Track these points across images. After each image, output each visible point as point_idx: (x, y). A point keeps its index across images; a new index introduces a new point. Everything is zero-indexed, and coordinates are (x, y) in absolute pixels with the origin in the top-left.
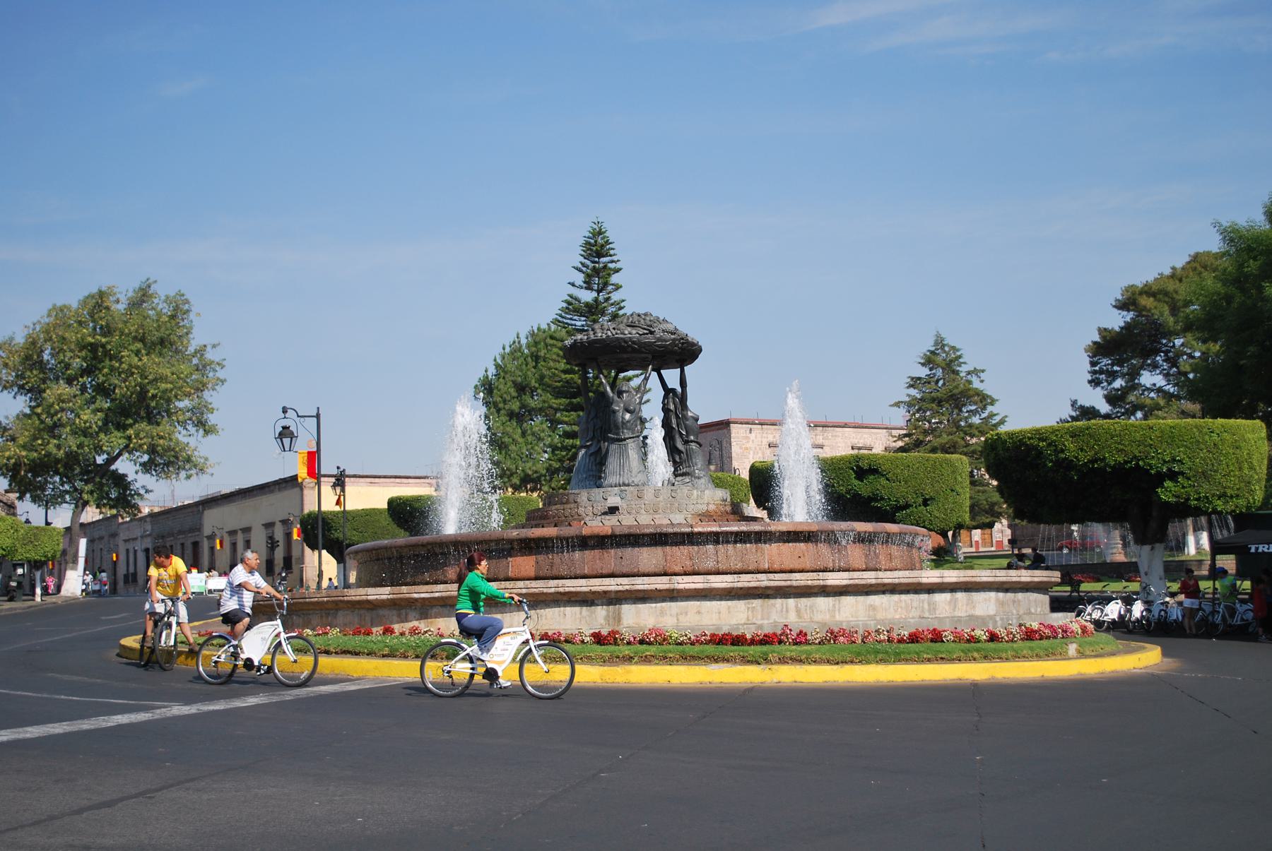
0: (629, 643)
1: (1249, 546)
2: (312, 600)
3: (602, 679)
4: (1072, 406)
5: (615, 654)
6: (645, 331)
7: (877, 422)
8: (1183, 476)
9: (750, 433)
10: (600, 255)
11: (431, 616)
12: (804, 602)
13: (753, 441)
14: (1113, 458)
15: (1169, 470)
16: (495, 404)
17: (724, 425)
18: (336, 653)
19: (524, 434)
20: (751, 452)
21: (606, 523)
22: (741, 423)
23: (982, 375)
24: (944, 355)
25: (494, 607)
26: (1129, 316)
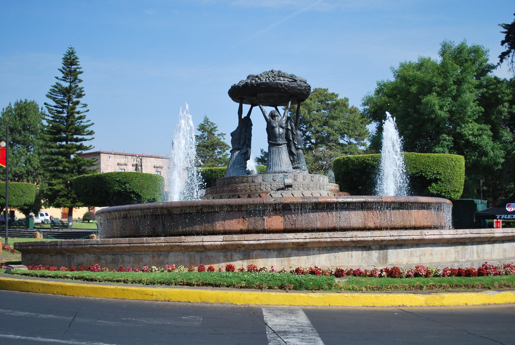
0: (408, 276)
1: (496, 215)
2: (151, 244)
3: (426, 304)
4: (261, 151)
5: (413, 284)
6: (293, 80)
8: (440, 181)
9: (110, 158)
10: (72, 64)
11: (252, 257)
12: (480, 247)
13: (110, 162)
15: (435, 178)
17: (98, 154)
18: (198, 285)
20: (110, 167)
21: (284, 195)
22: (106, 153)
23: (224, 136)
24: (208, 126)
25: (302, 250)
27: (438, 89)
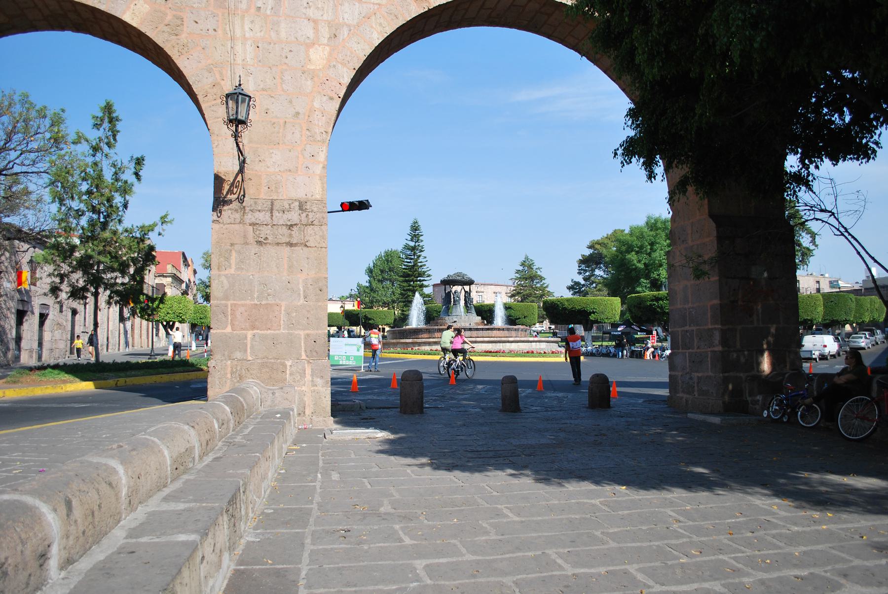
7: (503, 284)
10: (416, 230)
12: (504, 344)
14: (578, 307)
16: (373, 277)
19: (383, 287)
26: (591, 251)
27: (637, 249)
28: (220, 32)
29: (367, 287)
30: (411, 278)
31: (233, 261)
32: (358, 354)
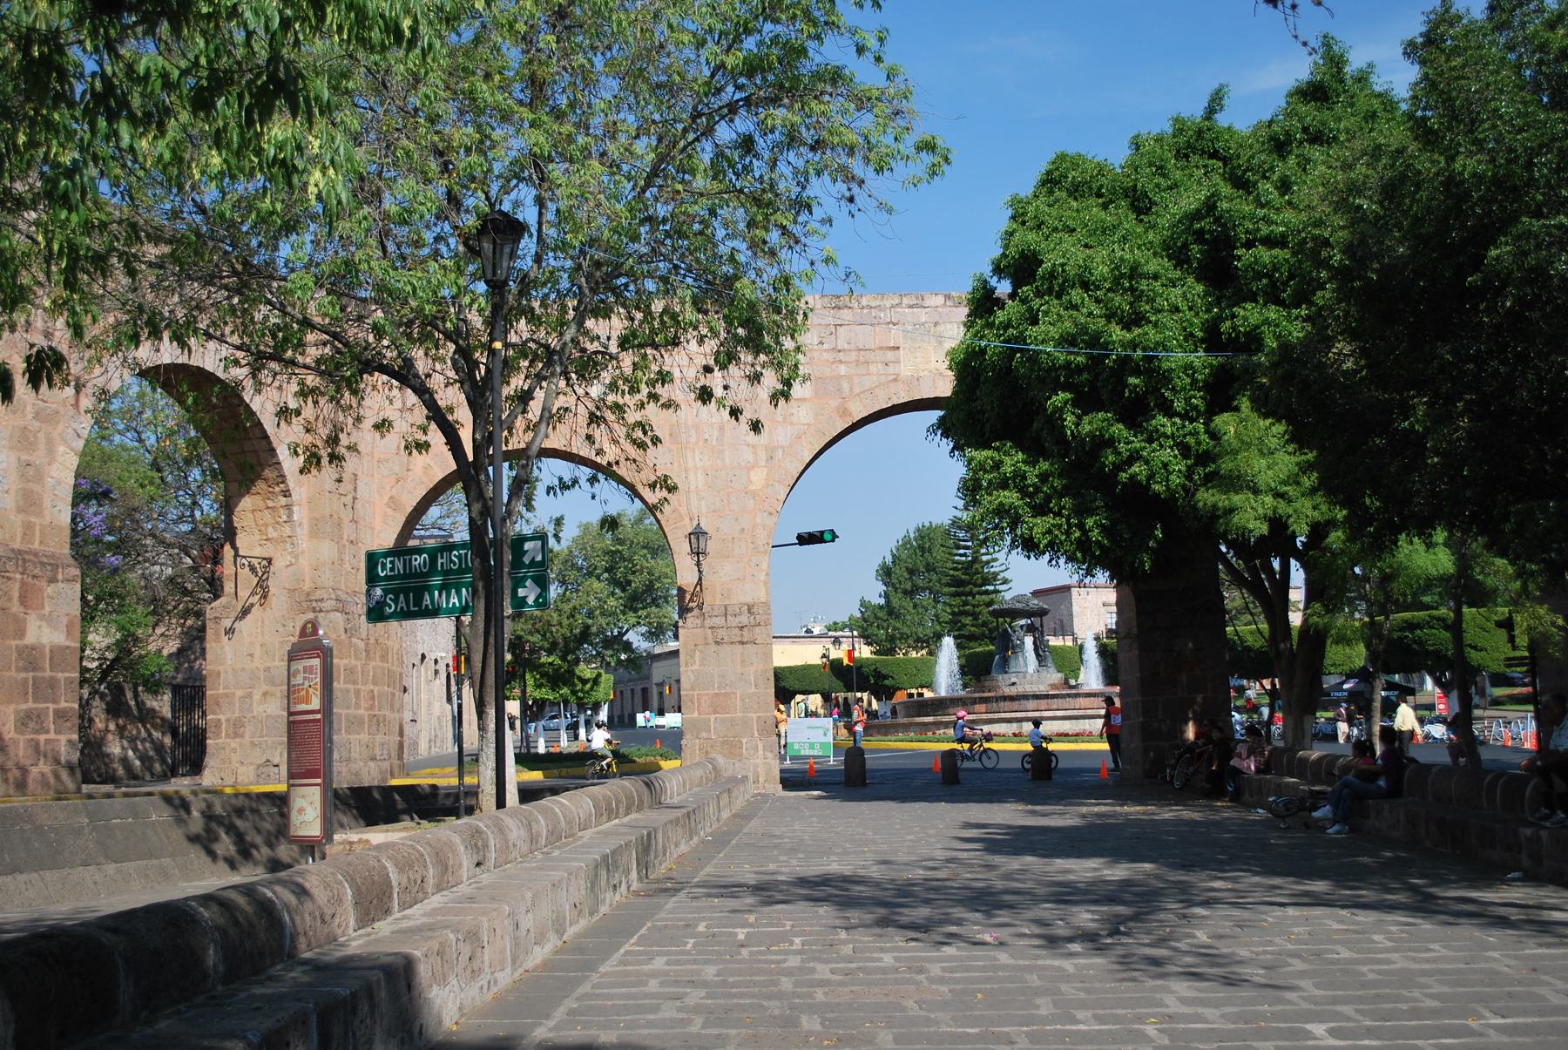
16: (893, 585)
19: (915, 606)
28: (675, 464)
29: (881, 607)
30: (967, 589)
31: (697, 659)
32: (824, 740)
